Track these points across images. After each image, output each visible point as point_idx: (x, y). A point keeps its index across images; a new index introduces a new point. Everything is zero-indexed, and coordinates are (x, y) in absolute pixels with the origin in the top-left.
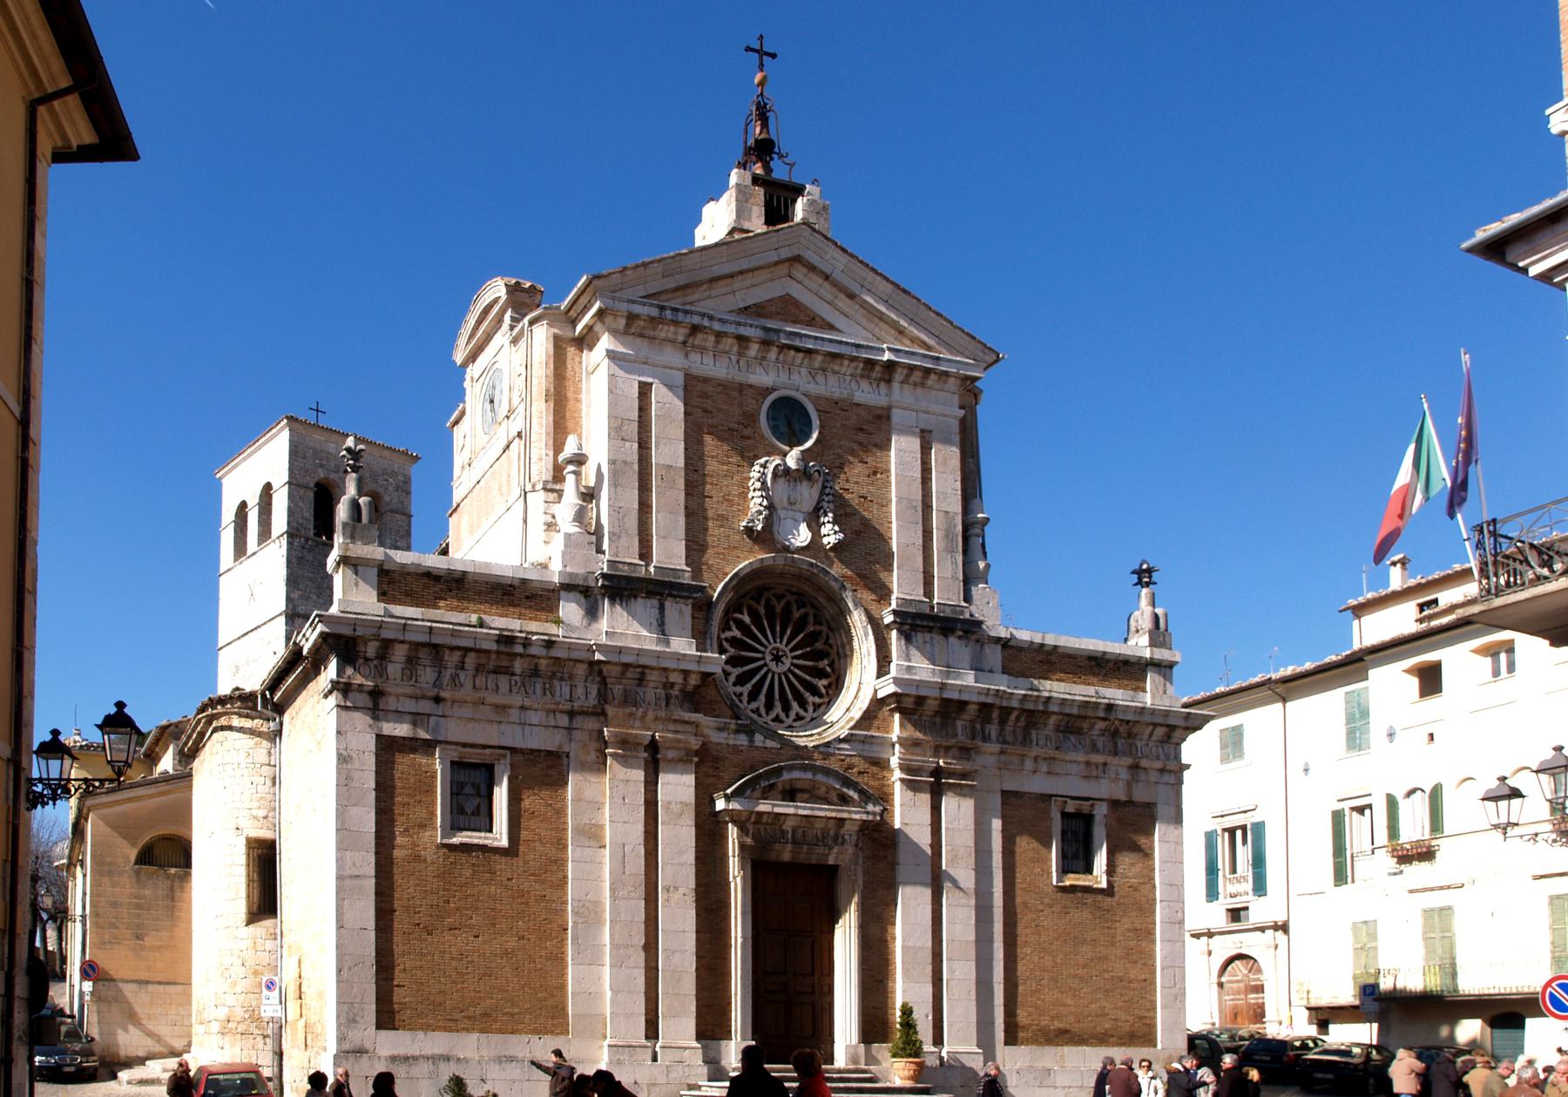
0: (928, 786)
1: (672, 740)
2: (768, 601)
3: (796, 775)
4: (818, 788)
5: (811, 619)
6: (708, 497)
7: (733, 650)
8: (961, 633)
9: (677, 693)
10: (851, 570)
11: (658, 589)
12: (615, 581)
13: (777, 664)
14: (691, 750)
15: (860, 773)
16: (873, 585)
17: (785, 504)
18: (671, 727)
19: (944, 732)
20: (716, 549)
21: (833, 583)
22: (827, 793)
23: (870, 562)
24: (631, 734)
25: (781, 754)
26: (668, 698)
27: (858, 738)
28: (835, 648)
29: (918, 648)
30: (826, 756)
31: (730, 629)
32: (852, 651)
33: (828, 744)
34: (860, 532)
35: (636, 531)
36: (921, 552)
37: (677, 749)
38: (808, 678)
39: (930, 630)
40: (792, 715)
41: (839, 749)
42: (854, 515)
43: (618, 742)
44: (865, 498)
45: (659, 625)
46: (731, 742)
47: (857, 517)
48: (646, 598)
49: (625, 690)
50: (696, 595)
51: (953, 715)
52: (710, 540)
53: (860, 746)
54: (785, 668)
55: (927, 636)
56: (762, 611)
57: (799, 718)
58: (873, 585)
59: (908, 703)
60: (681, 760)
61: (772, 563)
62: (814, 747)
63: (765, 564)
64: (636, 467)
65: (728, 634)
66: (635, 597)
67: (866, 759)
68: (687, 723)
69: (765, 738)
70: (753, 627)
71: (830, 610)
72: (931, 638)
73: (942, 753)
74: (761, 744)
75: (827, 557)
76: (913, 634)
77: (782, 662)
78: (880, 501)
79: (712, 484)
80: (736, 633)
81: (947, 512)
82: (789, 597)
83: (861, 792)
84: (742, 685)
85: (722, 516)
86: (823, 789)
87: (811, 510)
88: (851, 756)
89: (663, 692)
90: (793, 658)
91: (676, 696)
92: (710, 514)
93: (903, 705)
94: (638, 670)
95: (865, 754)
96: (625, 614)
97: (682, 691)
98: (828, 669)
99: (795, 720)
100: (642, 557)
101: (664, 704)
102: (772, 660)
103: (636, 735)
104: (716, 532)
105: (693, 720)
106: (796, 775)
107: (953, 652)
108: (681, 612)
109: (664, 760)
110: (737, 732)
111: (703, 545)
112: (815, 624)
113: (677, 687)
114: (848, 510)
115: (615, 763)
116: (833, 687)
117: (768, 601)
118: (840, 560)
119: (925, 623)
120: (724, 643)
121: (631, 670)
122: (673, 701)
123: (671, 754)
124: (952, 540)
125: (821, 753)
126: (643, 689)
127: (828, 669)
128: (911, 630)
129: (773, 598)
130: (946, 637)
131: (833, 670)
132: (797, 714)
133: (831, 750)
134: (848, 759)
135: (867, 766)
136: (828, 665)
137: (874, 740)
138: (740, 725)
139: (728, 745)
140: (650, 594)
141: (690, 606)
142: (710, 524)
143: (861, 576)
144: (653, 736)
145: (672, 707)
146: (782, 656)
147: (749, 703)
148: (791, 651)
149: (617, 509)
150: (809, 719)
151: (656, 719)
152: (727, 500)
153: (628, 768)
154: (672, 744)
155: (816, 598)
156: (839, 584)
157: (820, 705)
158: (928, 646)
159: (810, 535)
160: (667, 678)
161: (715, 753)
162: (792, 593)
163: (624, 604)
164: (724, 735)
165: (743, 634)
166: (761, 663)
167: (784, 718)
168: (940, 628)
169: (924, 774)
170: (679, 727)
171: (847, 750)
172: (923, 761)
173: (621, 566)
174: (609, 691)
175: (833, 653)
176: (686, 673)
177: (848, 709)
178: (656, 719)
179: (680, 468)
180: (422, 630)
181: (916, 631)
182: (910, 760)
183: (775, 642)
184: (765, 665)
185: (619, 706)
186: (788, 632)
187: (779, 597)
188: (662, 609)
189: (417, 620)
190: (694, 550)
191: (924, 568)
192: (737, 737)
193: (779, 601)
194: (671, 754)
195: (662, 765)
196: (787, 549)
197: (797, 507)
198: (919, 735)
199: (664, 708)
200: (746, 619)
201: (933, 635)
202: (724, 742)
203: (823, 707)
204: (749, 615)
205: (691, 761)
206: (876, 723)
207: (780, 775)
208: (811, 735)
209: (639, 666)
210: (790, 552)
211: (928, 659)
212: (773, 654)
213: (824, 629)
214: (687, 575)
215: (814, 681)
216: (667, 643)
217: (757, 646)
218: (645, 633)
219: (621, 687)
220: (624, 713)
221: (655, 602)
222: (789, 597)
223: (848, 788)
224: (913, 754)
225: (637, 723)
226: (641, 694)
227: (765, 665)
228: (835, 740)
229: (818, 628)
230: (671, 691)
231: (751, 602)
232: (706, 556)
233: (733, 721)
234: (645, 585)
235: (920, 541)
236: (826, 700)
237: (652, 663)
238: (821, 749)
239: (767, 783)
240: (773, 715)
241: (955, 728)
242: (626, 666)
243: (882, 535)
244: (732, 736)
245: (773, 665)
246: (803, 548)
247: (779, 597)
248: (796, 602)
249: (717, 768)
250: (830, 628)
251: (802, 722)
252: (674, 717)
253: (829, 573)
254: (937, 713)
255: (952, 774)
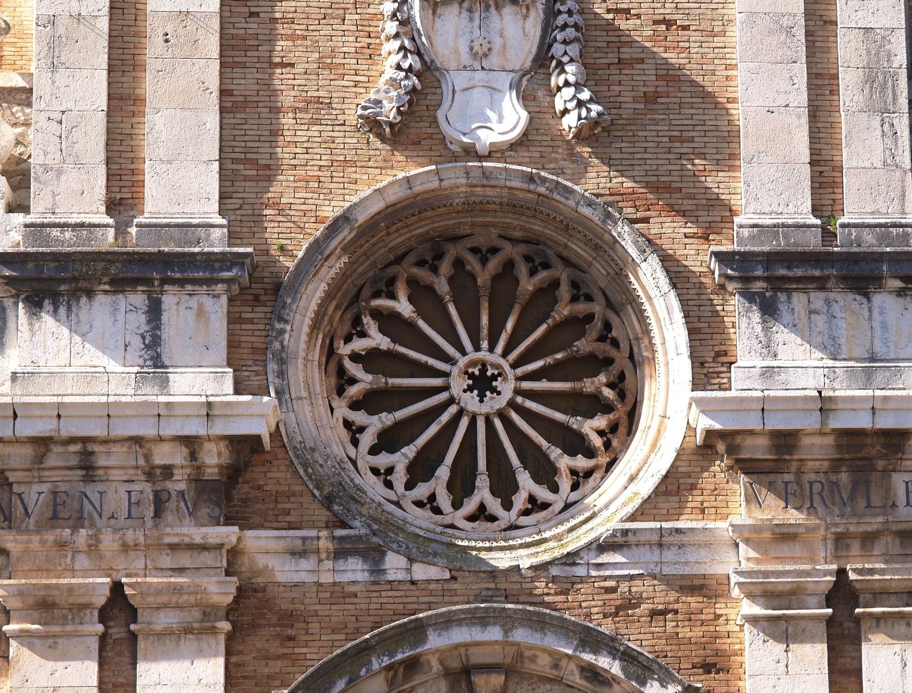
0: (822, 628)
1: (159, 591)
2: (459, 263)
3: (460, 635)
4: (533, 659)
5: (564, 291)
6: (283, 65)
7: (369, 378)
8: (898, 284)
9: (182, 486)
10: (633, 179)
11: (135, 272)
12: (30, 265)
13: (494, 390)
14: (214, 607)
15: (654, 613)
16: (687, 204)
17: (466, 59)
18: (166, 561)
19: (862, 503)
20: (301, 172)
21: (586, 211)
22: (556, 666)
23: (681, 156)
24: (57, 587)
25: (454, 593)
26: (160, 503)
27: (642, 538)
28: (624, 346)
29: (794, 327)
30: (567, 585)
31: (363, 334)
32: (654, 352)
33: (570, 559)
34: (657, 95)
35: (101, 156)
36: (805, 119)
37: (179, 607)
38: (559, 416)
39: (821, 284)
40: (520, 501)
41: (599, 566)
42: (642, 61)
43: (31, 608)
44: (669, 23)
45: (147, 347)
46: (326, 578)
47: (649, 66)
48: (115, 292)
49: (55, 493)
50: (226, 274)
51: (881, 464)
52: (284, 154)
53: (655, 555)
54: (500, 402)
55: (818, 299)
56: (442, 286)
57: (535, 505)
58: (687, 204)
59: (758, 449)
60: (188, 630)
61: (435, 184)
62: (534, 568)
63: (418, 189)
64: (103, 24)
65: (359, 345)
66: (90, 294)
67: (669, 581)
68: (204, 548)
69: (411, 560)
70: (421, 323)
71: (599, 271)
72: (828, 302)
73: (856, 549)
74: (401, 576)
75: (573, 156)
76: (782, 297)
77: (494, 390)
78: (704, 25)
79: (293, 37)
80: (377, 340)
81: (867, 30)
82: (509, 251)
83: (628, 657)
84: (392, 451)
85: (318, 100)
86: (544, 661)
87: (528, 64)
88: (632, 578)
89: (148, 488)
90: (519, 379)
91: (181, 494)
92: (287, 99)
93: (742, 456)
94: (73, 448)
95: (666, 571)
96: (66, 331)
97: (197, 481)
98: (608, 393)
99: (526, 513)
100: (112, 206)
101: (150, 512)
102: (470, 389)
103: (70, 589)
104: (302, 136)
105: (212, 541)
106: (460, 635)
107: (885, 327)
108: (201, 312)
109: (148, 634)
110: (339, 554)
111: (268, 167)
112: (574, 299)
113: (178, 474)
114: (626, 53)
115: (26, 652)
116: (622, 430)
117: (459, 263)
118: (608, 161)
119: (799, 272)
120: (348, 365)
121: (57, 449)
122: (172, 504)
123: (165, 620)
124: (884, 87)
125: (554, 579)
126: (100, 487)
127: (608, 393)
128: (776, 289)
129: (470, 258)
130: (867, 296)
131: (622, 395)
132: (532, 499)
133: (580, 571)
134: (624, 587)
135: (673, 596)
136: (610, 385)
137: (685, 539)
138: (342, 539)
139: (319, 585)
140: (120, 285)
141: (224, 299)
142: (287, 120)
143: (656, 188)
144: (841, 573)
145: (169, 517)
146: (494, 377)
147: (409, 486)
148: (514, 366)
149: (58, 116)
150: (560, 505)
151: (126, 548)
152: (330, 67)
153: (56, 659)
154: (163, 599)
155: (566, 246)
156: (600, 210)
157: (588, 474)
158: (820, 321)
159: (524, 115)
160: (147, 457)
161: (284, 606)
162: (513, 241)
163: (62, 311)
164: (306, 564)
165: (394, 341)
166: (443, 396)
167: (498, 511)
168: (843, 278)
169: (813, 601)
170: (185, 560)
171: (615, 565)
172: (800, 573)
173: (55, 232)
174: (14, 498)
175: (621, 360)
176: (190, 442)
177: (632, 479)
178: (126, 548)
179: (207, 15)
180: (800, 406)
181: (789, 292)
182: (766, 574)
183: (477, 348)
184: (451, 401)
185: (40, 528)
186: (510, 325)
187: (484, 254)
188: (154, 311)
189: (219, 396)
190: (246, 179)
191: (814, 152)
192: (341, 564)
193: (484, 261)
194: (165, 620)
195: (141, 645)
196: (470, 152)
197: (494, 61)
198: (794, 516)
199: (149, 523)
200: (404, 307)
201: (832, 295)
202: (309, 578)
203: (597, 475)
204: (411, 300)
205: (213, 631)
206: (694, 501)
207: (423, 640)
208: (544, 541)
209: (73, 440)
210: (481, 158)
211: (823, 348)
212: (471, 376)
213: (597, 308)
214: (217, 233)
215: (575, 422)
216: (164, 383)
217: (432, 362)
218: (114, 366)
219: (45, 487)
220: (43, 542)
221: (138, 299)
222: (509, 251)
223: (595, 652)
224: (781, 559)
225: (82, 562)
226: (95, 498)
227: (451, 401)
228: (588, 546)
229: (582, 308)
230: (169, 485)
231: (415, 270)
232: (275, 188)
233: (324, 533)
234: (100, 266)
235: (802, 98)
236: (603, 460)
237: (97, 430)
238: (554, 571)
239: (386, 661)
240: (470, 506)
241: (888, 489)
242: (42, 443)
243: (711, 95)
244: (329, 564)
245: (471, 402)
246: (514, 146)
247: (484, 254)
248: (528, 259)
249: (291, 638)
250: (609, 304)
251: (544, 514)
252: (167, 540)
253: (572, 191)
254: (836, 465)
255: (880, 595)
